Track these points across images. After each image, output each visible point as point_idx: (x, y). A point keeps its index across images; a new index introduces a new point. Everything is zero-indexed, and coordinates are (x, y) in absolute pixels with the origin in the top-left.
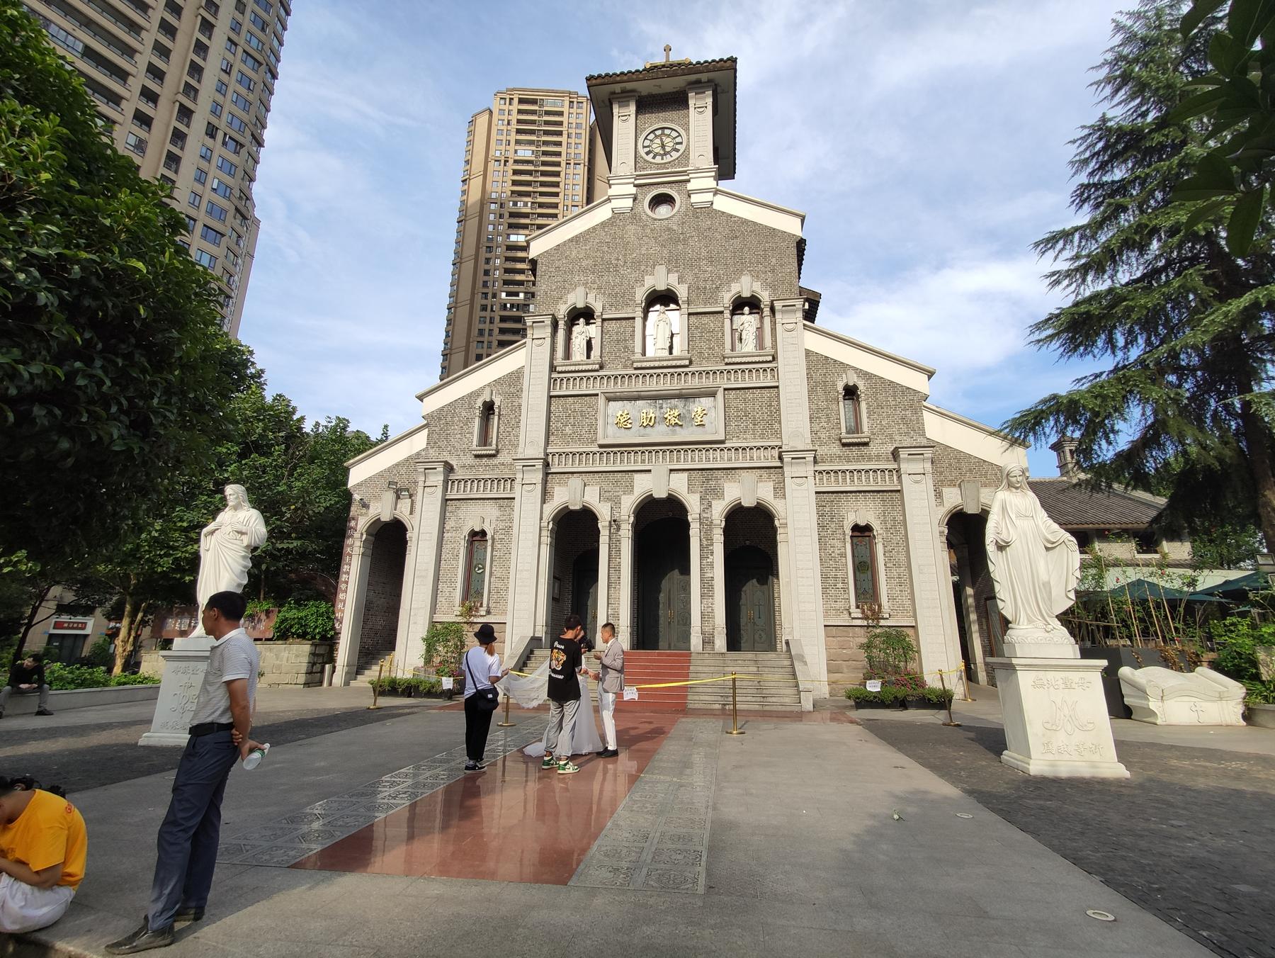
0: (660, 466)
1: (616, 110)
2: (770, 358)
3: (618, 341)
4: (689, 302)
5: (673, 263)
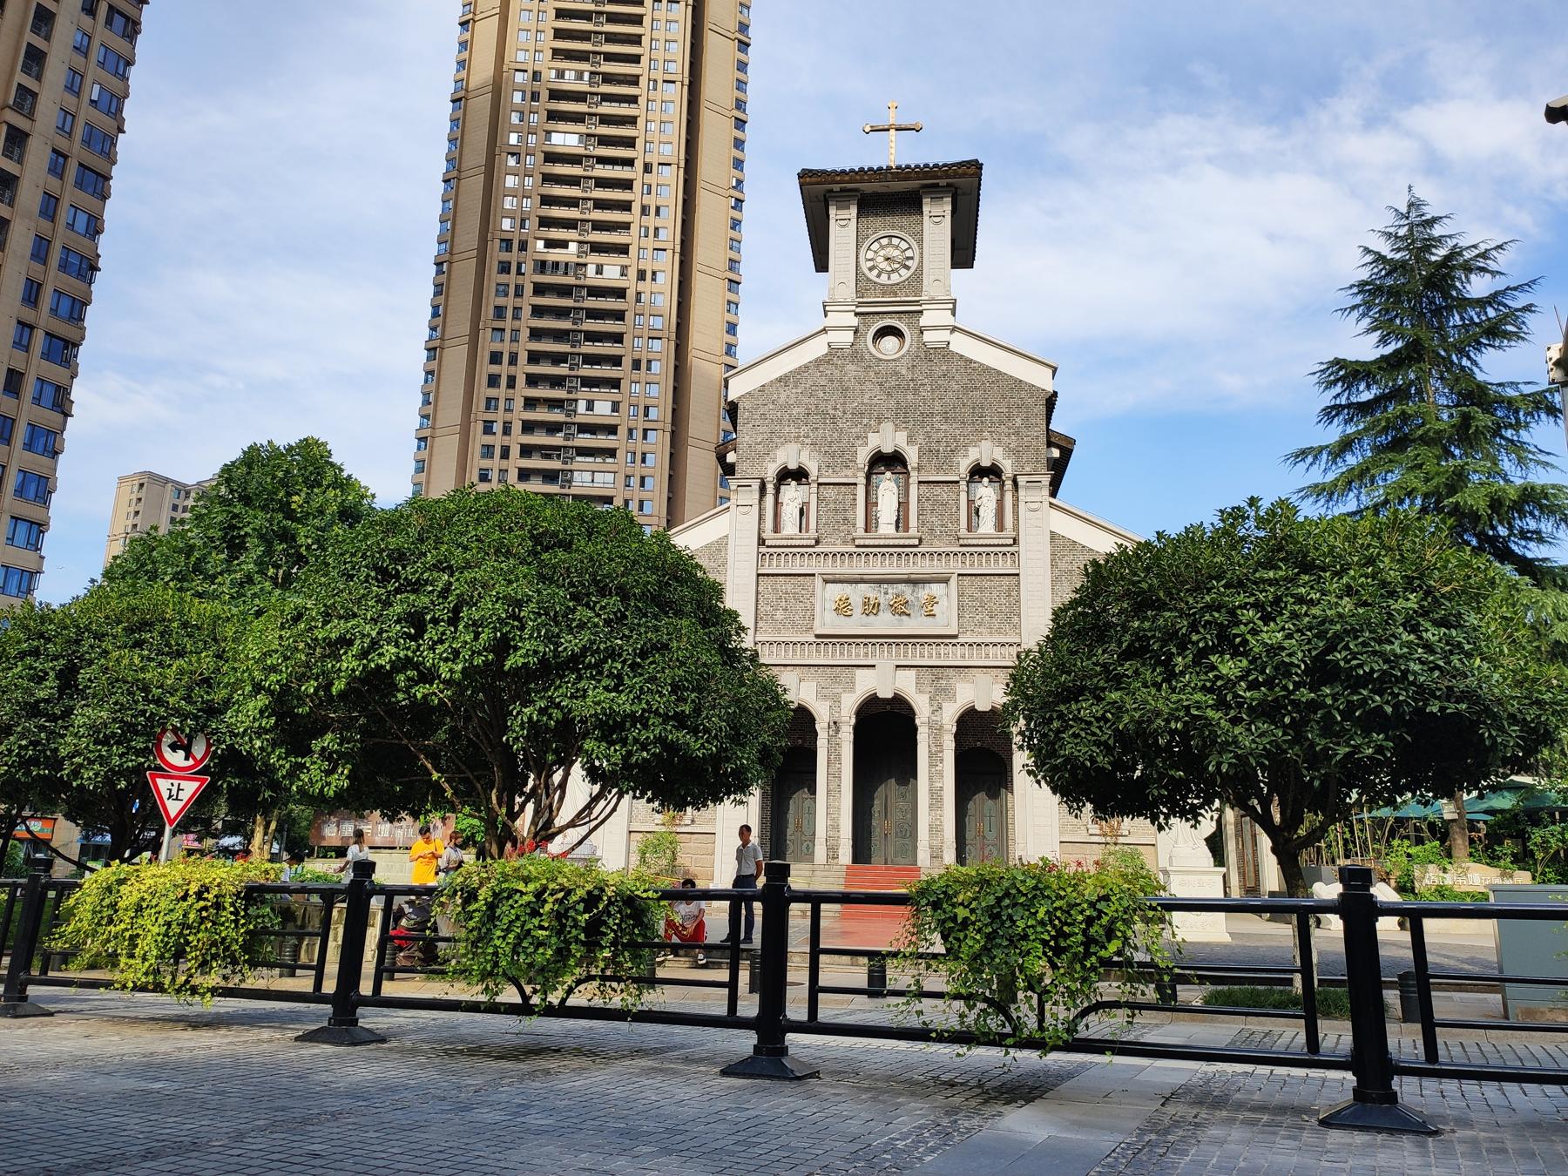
0: (885, 659)
1: (832, 211)
2: (1011, 541)
3: (836, 510)
4: (919, 469)
5: (902, 417)
